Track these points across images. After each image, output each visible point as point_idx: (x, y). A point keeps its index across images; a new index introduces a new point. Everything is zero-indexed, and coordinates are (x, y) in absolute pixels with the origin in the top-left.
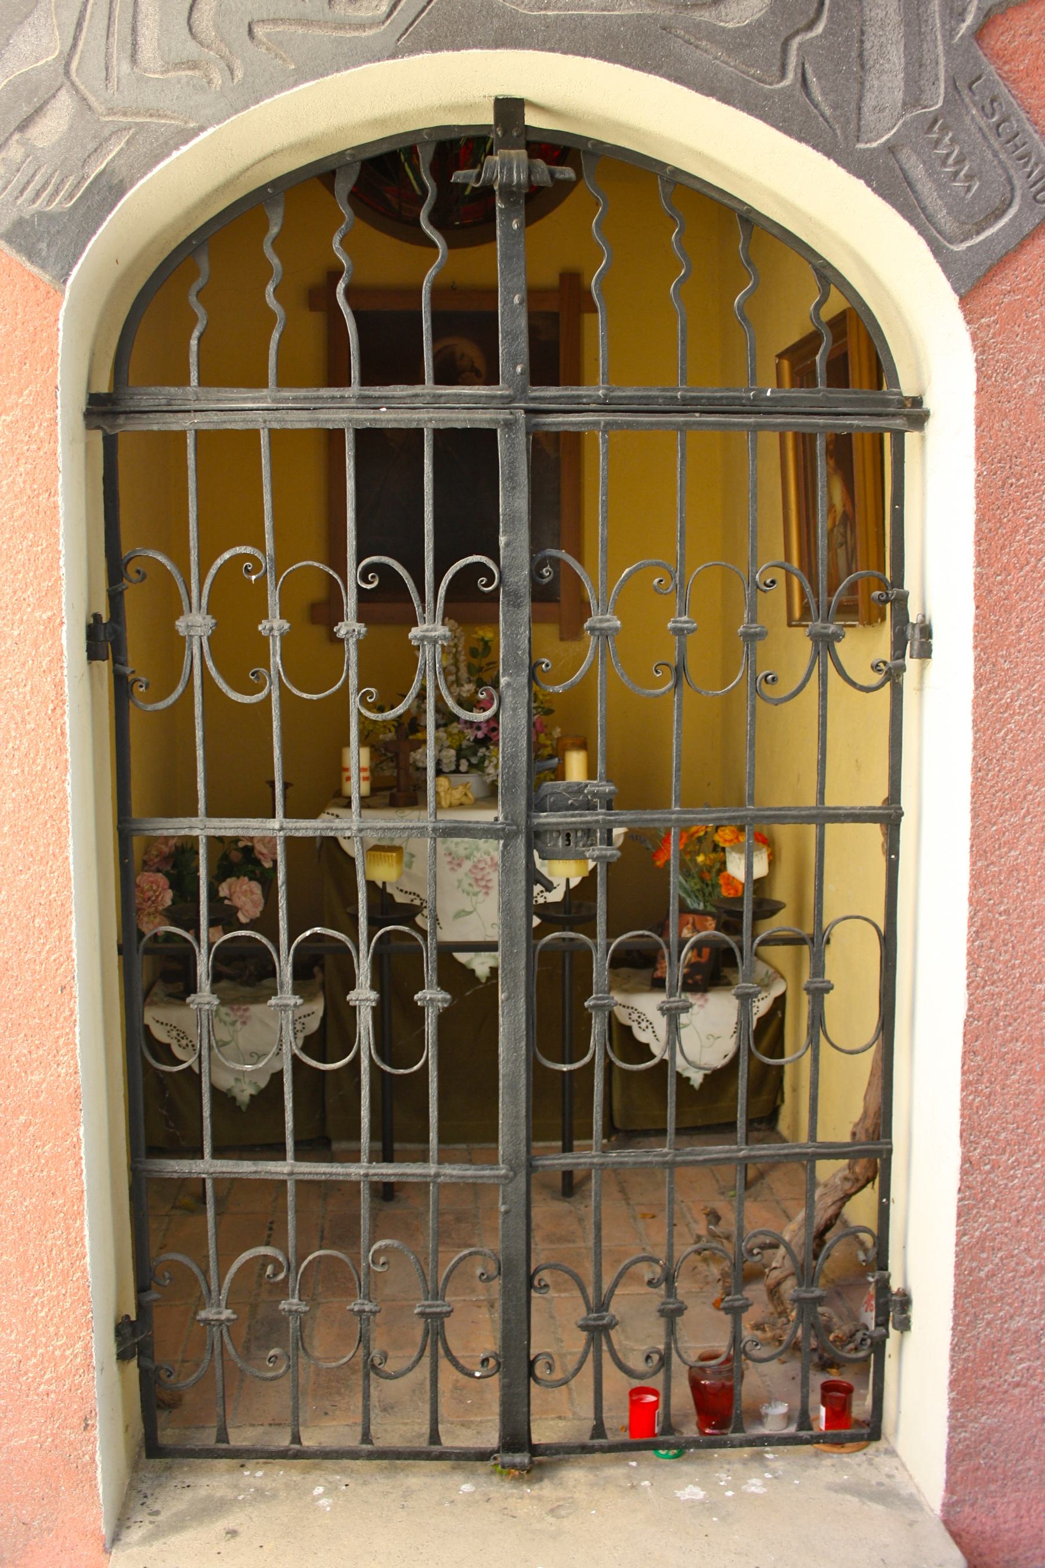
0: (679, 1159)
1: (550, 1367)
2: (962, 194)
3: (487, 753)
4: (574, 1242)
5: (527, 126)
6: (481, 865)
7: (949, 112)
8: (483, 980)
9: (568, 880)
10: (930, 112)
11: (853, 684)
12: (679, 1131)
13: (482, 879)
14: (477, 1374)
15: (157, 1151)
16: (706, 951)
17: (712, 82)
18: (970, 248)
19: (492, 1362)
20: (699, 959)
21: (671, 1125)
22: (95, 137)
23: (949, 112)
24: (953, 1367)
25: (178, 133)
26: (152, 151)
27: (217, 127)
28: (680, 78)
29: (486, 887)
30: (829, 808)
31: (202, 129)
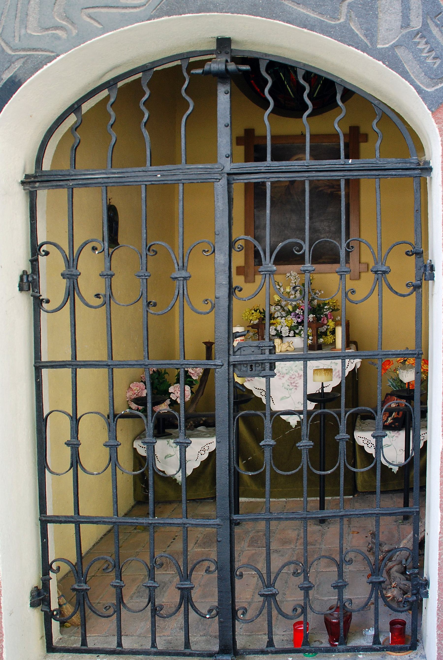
0: (308, 516)
1: (243, 614)
2: (432, 66)
3: (302, 328)
4: (315, 545)
5: (217, 48)
6: (293, 377)
7: (425, 30)
8: (294, 427)
9: (322, 383)
10: (415, 30)
11: (396, 293)
12: (382, 492)
13: (294, 383)
14: (208, 616)
15: (42, 514)
16: (401, 413)
17: (305, 22)
18: (437, 90)
19: (214, 612)
20: (398, 416)
21: (378, 491)
22: (8, 62)
23: (425, 30)
24: (438, 618)
25: (47, 58)
26: (34, 66)
27: (65, 54)
28: (289, 21)
29: (296, 386)
30: (80, 361)
31: (58, 56)
